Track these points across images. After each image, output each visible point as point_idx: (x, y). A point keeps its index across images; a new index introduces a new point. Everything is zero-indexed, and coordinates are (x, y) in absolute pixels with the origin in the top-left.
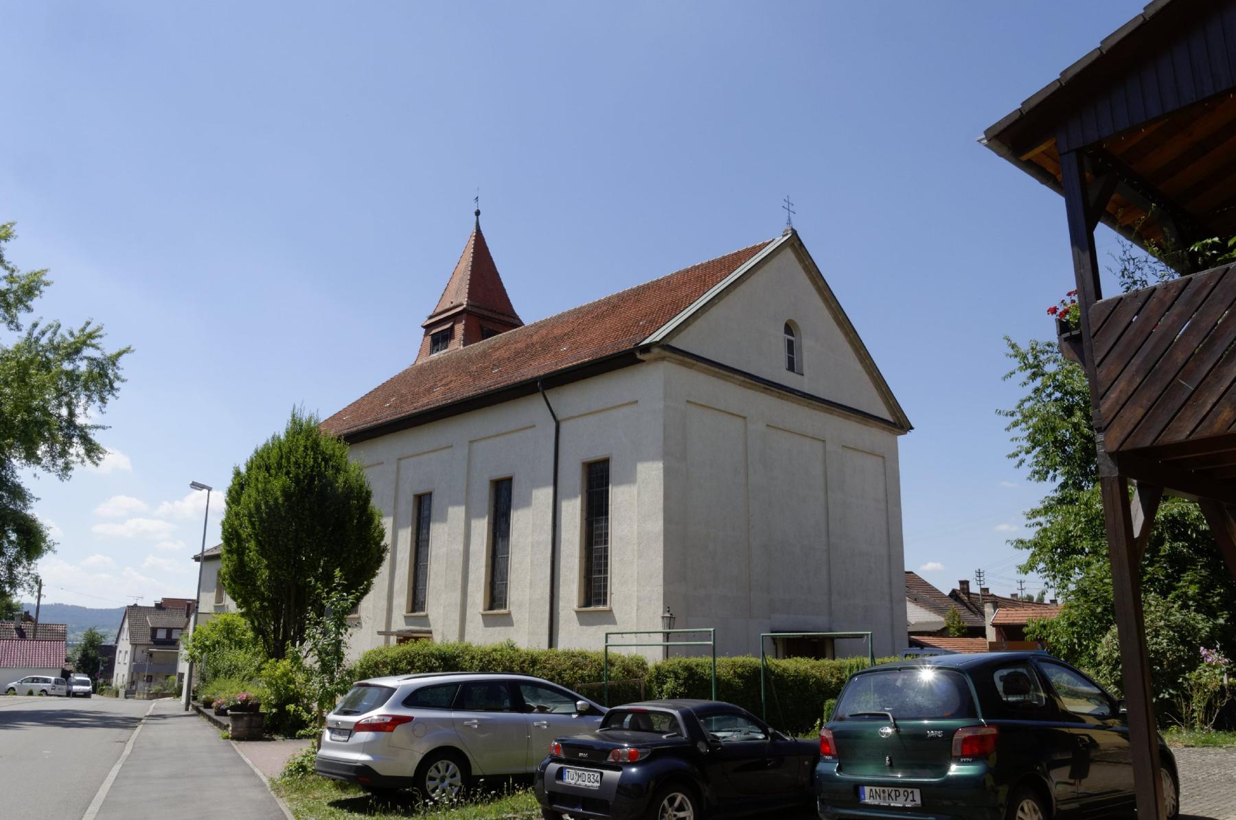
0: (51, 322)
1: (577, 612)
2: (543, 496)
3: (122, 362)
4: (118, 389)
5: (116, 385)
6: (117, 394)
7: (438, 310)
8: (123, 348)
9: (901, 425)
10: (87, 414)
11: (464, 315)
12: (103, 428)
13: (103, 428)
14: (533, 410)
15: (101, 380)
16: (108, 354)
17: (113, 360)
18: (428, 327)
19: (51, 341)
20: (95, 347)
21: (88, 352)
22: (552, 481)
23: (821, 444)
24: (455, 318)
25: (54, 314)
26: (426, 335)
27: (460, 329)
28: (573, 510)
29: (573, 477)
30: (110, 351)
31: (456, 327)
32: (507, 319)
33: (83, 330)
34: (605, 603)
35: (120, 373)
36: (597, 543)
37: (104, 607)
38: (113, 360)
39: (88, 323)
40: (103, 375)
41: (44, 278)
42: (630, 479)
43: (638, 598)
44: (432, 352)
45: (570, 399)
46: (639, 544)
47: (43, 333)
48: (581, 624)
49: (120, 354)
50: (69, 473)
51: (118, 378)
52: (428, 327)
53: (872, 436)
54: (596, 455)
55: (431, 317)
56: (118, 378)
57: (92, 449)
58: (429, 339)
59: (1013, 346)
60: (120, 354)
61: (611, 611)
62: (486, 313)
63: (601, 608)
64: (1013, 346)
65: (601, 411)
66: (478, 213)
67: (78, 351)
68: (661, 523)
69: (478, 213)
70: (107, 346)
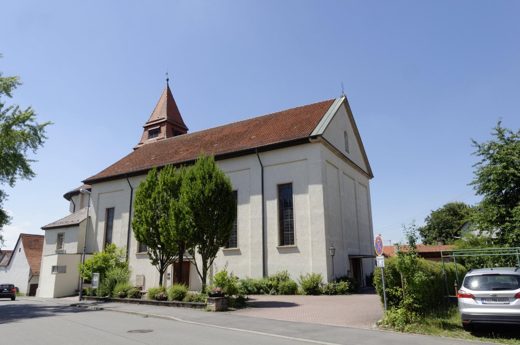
0: (12, 105)
1: (277, 248)
2: (257, 199)
3: (45, 128)
4: (44, 142)
5: (42, 140)
6: (43, 144)
7: (150, 121)
8: (47, 122)
9: (370, 175)
10: (28, 154)
11: (166, 123)
12: (34, 161)
13: (34, 161)
14: (252, 161)
15: (35, 137)
16: (39, 124)
17: (41, 128)
18: (146, 128)
19: (13, 114)
20: (32, 120)
21: (28, 122)
22: (261, 192)
23: (353, 181)
24: (161, 124)
25: (15, 102)
26: (145, 130)
27: (164, 129)
28: (273, 206)
29: (272, 190)
30: (41, 123)
31: (162, 128)
32: (182, 126)
33: (27, 111)
34: (236, 246)
35: (44, 134)
36: (286, 218)
37: (325, 250)
38: (41, 128)
39: (29, 108)
40: (36, 134)
41: (18, 81)
42: (304, 191)
43: (312, 241)
44: (149, 138)
45: (268, 158)
46: (311, 219)
47: (8, 110)
48: (280, 253)
49: (45, 125)
50: (14, 183)
51: (44, 137)
52: (146, 128)
53: (361, 178)
54: (285, 180)
55: (147, 123)
56: (44, 137)
57: (28, 172)
58: (147, 132)
59: (475, 142)
60: (45, 125)
61: (239, 250)
62: (173, 122)
63: (234, 248)
64: (475, 142)
65: (287, 163)
66: (168, 80)
67: (24, 122)
68: (322, 210)
69: (168, 80)
70: (38, 121)
